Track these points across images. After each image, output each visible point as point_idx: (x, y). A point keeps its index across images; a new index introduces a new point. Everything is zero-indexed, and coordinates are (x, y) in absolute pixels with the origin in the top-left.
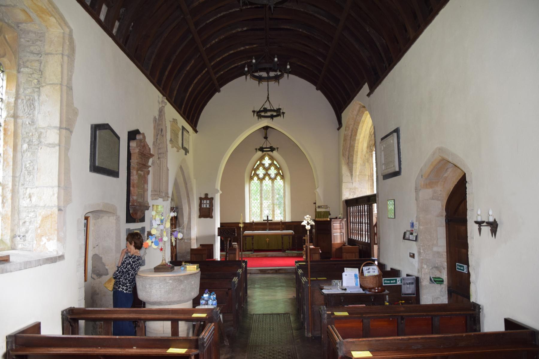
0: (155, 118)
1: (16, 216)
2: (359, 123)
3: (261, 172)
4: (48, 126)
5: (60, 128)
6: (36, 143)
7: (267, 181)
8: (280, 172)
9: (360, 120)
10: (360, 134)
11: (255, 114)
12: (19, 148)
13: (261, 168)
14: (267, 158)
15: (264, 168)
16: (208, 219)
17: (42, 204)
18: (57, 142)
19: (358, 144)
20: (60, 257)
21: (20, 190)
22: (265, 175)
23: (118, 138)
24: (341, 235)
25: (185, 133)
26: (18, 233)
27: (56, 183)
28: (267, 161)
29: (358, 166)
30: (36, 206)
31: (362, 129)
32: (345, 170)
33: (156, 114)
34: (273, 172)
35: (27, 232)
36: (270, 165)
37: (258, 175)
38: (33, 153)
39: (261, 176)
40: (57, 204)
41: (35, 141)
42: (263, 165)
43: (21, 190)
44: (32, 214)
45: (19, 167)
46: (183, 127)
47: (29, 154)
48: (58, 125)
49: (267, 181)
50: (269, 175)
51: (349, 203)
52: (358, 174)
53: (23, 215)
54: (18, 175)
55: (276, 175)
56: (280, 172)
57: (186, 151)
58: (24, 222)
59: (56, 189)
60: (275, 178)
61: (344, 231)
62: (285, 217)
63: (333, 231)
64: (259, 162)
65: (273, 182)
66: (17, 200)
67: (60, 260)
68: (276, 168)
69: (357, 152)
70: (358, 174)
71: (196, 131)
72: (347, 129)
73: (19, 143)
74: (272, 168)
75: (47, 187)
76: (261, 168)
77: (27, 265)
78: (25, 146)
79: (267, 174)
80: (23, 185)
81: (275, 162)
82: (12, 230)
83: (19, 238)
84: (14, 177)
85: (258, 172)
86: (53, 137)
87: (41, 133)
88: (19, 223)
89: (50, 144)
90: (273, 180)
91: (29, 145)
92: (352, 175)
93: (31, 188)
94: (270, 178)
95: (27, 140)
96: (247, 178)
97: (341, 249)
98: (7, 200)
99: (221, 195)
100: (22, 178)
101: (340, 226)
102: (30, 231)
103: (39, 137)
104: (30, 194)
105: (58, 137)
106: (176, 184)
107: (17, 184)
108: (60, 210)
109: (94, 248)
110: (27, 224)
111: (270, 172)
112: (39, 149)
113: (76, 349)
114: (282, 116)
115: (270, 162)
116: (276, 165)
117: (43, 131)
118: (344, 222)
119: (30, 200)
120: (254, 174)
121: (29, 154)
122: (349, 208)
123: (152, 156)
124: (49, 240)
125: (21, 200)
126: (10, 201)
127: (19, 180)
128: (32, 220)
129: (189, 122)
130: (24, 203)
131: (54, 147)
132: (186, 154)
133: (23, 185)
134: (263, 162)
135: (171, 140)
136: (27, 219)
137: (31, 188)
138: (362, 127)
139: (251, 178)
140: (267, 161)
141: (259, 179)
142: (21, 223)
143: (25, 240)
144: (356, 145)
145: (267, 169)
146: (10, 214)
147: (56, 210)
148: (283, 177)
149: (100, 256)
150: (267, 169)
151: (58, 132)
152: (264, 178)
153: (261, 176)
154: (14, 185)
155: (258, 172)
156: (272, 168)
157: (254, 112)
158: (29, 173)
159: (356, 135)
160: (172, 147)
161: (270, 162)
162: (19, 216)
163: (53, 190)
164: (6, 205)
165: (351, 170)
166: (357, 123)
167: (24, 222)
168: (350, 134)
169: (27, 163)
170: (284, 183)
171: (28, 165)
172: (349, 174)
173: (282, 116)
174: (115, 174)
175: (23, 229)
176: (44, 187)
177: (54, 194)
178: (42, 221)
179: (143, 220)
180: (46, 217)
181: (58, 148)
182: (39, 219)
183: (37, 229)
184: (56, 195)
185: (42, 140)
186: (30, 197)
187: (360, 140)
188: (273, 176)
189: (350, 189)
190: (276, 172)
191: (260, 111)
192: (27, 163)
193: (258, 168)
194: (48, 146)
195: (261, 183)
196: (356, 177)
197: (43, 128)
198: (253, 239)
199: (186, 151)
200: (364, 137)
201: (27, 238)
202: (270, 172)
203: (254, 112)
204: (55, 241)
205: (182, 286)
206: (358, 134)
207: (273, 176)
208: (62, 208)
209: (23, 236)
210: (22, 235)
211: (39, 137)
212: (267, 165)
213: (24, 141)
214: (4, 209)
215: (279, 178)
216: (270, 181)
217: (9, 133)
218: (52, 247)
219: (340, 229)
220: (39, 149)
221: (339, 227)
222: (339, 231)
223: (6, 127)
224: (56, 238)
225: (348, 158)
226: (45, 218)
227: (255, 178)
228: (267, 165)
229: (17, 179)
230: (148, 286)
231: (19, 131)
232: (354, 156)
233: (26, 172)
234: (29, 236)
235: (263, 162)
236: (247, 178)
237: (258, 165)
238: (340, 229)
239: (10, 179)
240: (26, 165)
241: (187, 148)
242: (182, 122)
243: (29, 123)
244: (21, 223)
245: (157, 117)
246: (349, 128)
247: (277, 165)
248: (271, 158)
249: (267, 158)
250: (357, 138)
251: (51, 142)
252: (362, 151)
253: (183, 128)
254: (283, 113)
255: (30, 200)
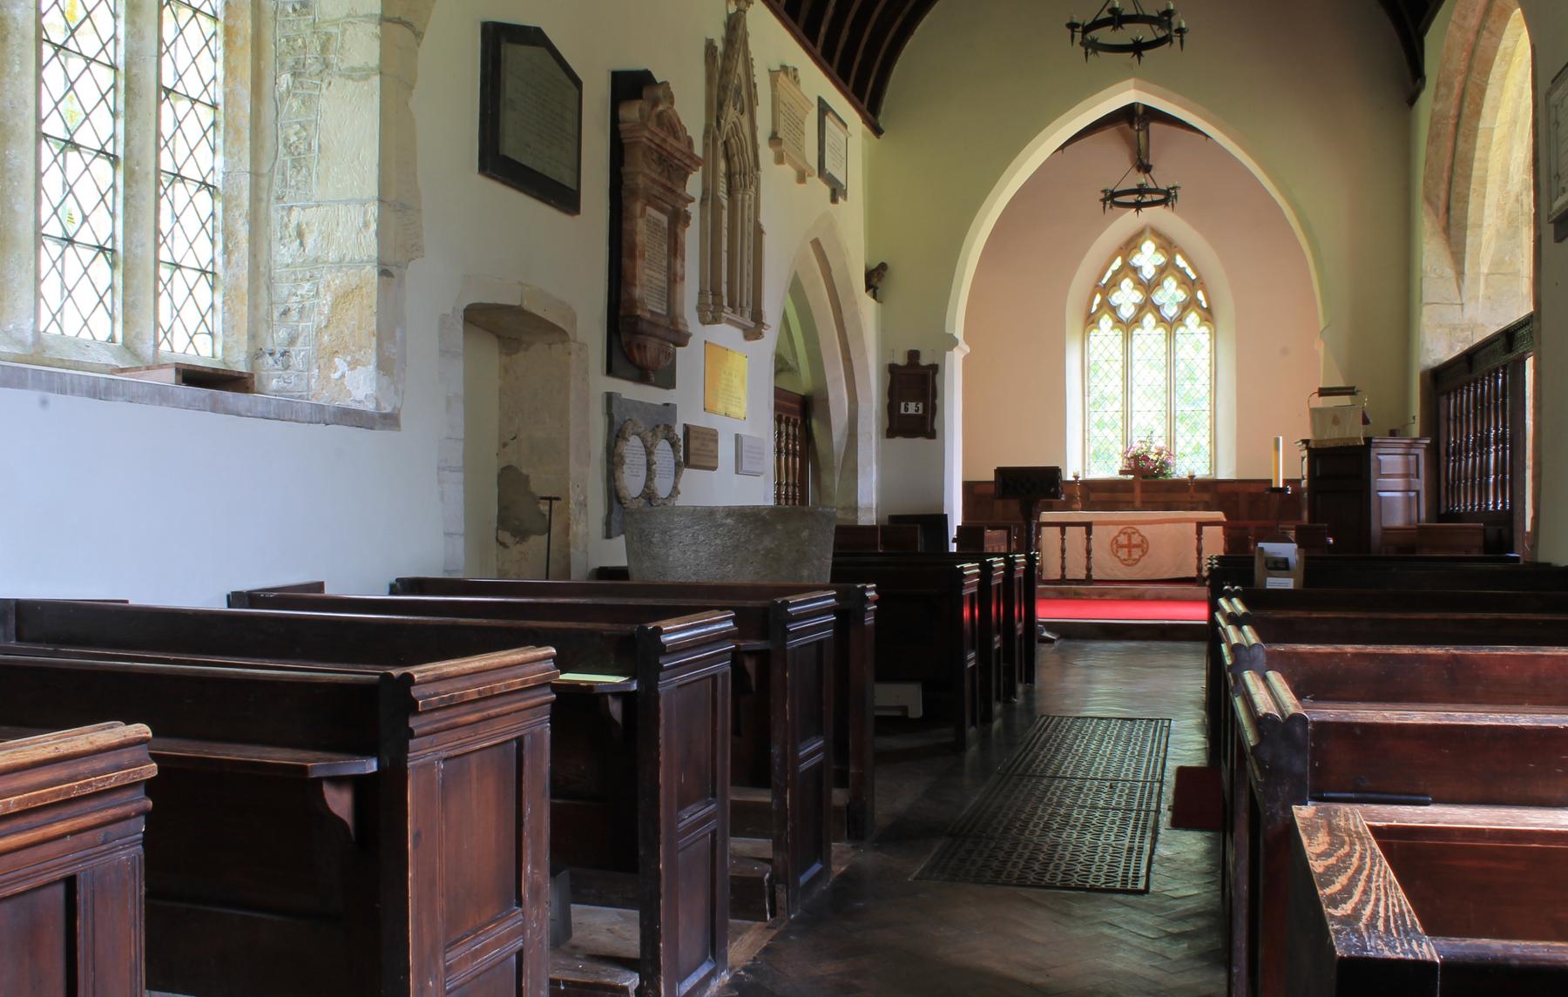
0: (710, 47)
1: (264, 292)
2: (1488, 64)
3: (1127, 297)
4: (348, 16)
5: (384, 20)
6: (316, 68)
7: (1149, 334)
8: (1200, 295)
9: (1496, 48)
10: (1496, 109)
11: (1078, 36)
12: (267, 84)
13: (1127, 284)
14: (1148, 246)
15: (1140, 284)
16: (920, 441)
17: (333, 256)
18: (374, 61)
19: (1487, 148)
20: (385, 416)
21: (273, 214)
22: (1141, 308)
23: (578, 83)
24: (1409, 499)
25: (830, 123)
26: (269, 346)
27: (372, 190)
28: (1148, 258)
29: (1485, 238)
30: (316, 260)
31: (1502, 88)
32: (1431, 252)
33: (718, 34)
34: (1170, 295)
35: (292, 341)
36: (1162, 271)
37: (1114, 310)
38: (307, 101)
39: (1127, 312)
40: (375, 254)
41: (313, 66)
42: (1136, 270)
43: (276, 213)
44: (307, 286)
45: (268, 144)
46: (820, 100)
47: (295, 105)
48: (377, 11)
49: (1149, 334)
50: (1157, 309)
51: (1441, 379)
52: (1485, 269)
53: (283, 289)
54: (265, 169)
55: (1185, 307)
56: (1200, 295)
57: (837, 191)
58: (285, 313)
59: (373, 210)
60: (1180, 320)
61: (1420, 484)
62: (1214, 463)
63: (1377, 483)
64: (1118, 262)
65: (1171, 336)
66: (266, 246)
67: (384, 427)
68: (1184, 281)
69: (1483, 183)
70: (1485, 269)
71: (877, 131)
72: (1443, 90)
73: (268, 73)
74: (1170, 283)
75: (347, 203)
76: (1127, 284)
77: (286, 412)
78: (285, 79)
79: (1147, 305)
80: (280, 199)
81: (1180, 261)
82: (253, 336)
83: (270, 360)
84: (255, 174)
85: (1116, 298)
86: (363, 47)
87: (329, 36)
88: (270, 314)
89: (353, 69)
90: (1171, 325)
91: (294, 75)
92: (1460, 274)
93: (304, 209)
94: (1161, 320)
95: (290, 61)
96: (1073, 320)
97: (1407, 545)
98: (236, 244)
99: (966, 360)
100: (277, 178)
101: (1407, 464)
102: (301, 340)
103: (324, 48)
104: (299, 225)
105: (375, 47)
106: (796, 289)
107: (265, 196)
108: (384, 273)
109: (505, 445)
110: (294, 315)
111: (1159, 297)
112: (324, 86)
113: (509, 922)
114: (1176, 40)
115: (1161, 259)
116: (1182, 271)
117: (333, 30)
118: (1421, 453)
119: (302, 244)
120: (1100, 306)
121: (295, 105)
122: (1444, 399)
123: (697, 162)
124: (353, 365)
125: (276, 246)
126: (244, 246)
127: (270, 185)
128: (307, 304)
129: (834, 71)
130: (284, 253)
131: (366, 78)
132: (834, 200)
133: (280, 199)
134: (1137, 260)
135: (774, 139)
136: (293, 303)
137: (304, 209)
138: (1504, 77)
139: (1091, 320)
140: (1148, 258)
141: (1118, 322)
142: (276, 315)
143: (287, 367)
144: (1478, 154)
145: (1149, 287)
146: (245, 285)
147: (371, 272)
148: (1208, 316)
149: (524, 471)
150: (1149, 287)
151: (378, 30)
152: (1136, 320)
153: (1127, 312)
154: (255, 199)
155: (1116, 298)
156: (1170, 283)
157: (1072, 26)
158: (297, 164)
159: (1477, 113)
160: (779, 160)
161: (1161, 259)
162: (269, 293)
163: (365, 213)
164: (233, 259)
165: (1457, 254)
166: (1478, 64)
167: (285, 313)
168: (1453, 112)
169: (291, 132)
170: (1214, 337)
171: (293, 139)
172: (1449, 272)
173: (1176, 40)
174: (565, 198)
175: (282, 334)
176: (339, 202)
177: (366, 225)
178: (334, 306)
179: (669, 382)
180: (346, 295)
181: (376, 80)
182: (326, 300)
183: (319, 331)
184: (373, 227)
185: (333, 58)
186: (300, 235)
187: (1497, 135)
188: (1170, 311)
189: (1454, 328)
190: (1181, 295)
191: (1097, 24)
192: (291, 132)
193: (1114, 284)
194: (349, 77)
195: (1127, 338)
196: (1476, 281)
197: (335, 23)
198: (1089, 532)
199: (837, 191)
200: (1514, 122)
201: (293, 361)
202: (1159, 297)
203: (1072, 26)
204: (371, 368)
205: (767, 542)
206: (1486, 111)
207: (1170, 311)
208: (393, 270)
209: (283, 355)
210: (279, 350)
211: (324, 48)
212: (1148, 272)
213: (282, 64)
214: (230, 272)
215: (1193, 318)
216: (1161, 330)
217: (240, 42)
218: (359, 385)
219: (1406, 475)
220: (324, 86)
221: (1400, 470)
222: (1399, 483)
223: (231, 22)
224: (373, 359)
225: (1448, 209)
226: (343, 297)
227: (1106, 321)
228: (1148, 272)
229: (264, 182)
230: (656, 538)
231: (268, 35)
232: (1473, 199)
233: (288, 159)
234: (297, 359)
235: (1137, 260)
236: (1073, 320)
237: (1116, 273)
238: (1406, 475)
239: (245, 180)
240: (287, 139)
241: (842, 180)
242: (816, 83)
243: (294, 10)
244: (276, 315)
245: (720, 45)
246: (1450, 86)
247: (1189, 271)
248: (1167, 245)
249: (1148, 246)
250: (1483, 125)
251: (356, 64)
252: (1505, 182)
253: (824, 109)
254: (1180, 31)
255: (302, 244)
